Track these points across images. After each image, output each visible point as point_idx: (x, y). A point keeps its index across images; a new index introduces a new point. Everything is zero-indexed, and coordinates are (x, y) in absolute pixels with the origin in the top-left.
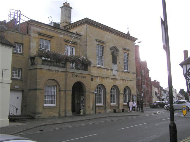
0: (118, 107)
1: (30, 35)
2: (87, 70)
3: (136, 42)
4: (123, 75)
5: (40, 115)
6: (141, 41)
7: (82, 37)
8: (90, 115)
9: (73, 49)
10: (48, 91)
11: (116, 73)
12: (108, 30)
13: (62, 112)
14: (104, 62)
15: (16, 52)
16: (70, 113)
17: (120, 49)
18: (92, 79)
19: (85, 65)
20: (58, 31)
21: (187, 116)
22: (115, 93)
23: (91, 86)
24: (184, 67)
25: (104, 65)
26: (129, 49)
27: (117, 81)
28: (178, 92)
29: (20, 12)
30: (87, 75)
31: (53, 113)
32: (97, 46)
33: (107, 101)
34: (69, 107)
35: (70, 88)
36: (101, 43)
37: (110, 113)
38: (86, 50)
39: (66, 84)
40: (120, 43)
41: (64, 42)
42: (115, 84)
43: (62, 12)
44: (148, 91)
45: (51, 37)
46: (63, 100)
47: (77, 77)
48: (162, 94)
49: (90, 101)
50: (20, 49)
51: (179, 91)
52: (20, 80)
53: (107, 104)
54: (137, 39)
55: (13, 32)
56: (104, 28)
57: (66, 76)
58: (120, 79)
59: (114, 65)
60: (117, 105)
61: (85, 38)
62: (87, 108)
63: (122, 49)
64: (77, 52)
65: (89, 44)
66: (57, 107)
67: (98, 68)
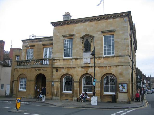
4: (100, 61)
14: (63, 52)
17: (98, 36)
18: (57, 71)
26: (115, 29)
41: (43, 46)
47: (38, 70)
67: (64, 60)
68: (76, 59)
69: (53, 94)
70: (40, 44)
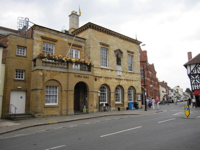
0: (123, 105)
1: (33, 39)
2: (90, 71)
3: (141, 45)
4: (127, 75)
5: (40, 114)
6: (145, 44)
7: (86, 40)
8: (93, 112)
9: (78, 52)
10: (49, 91)
11: (121, 74)
12: (112, 34)
13: (64, 110)
14: (108, 63)
15: (19, 54)
16: (72, 111)
17: (125, 52)
18: (96, 80)
19: (89, 67)
20: (62, 35)
21: (191, 117)
22: (120, 92)
23: (94, 86)
24: (188, 67)
25: (108, 66)
26: (134, 52)
27: (122, 81)
28: (184, 91)
29: (28, 19)
30: (90, 76)
31: (54, 112)
32: (101, 48)
33: (111, 99)
34: (72, 106)
35: (72, 87)
36: (105, 46)
37: (114, 110)
38: (89, 53)
39: (68, 84)
40: (125, 47)
42: (120, 84)
43: (70, 20)
44: (155, 91)
45: (55, 41)
46: (64, 100)
47: (79, 77)
48: (169, 92)
49: (93, 100)
50: (24, 51)
51: (186, 90)
52: (24, 81)
53: (111, 103)
54: (141, 42)
55: (16, 36)
56: (107, 32)
57: (68, 76)
58: (125, 80)
59: (118, 66)
60: (122, 103)
61: (89, 42)
62: (90, 107)
63: (126, 51)
64: (82, 54)
65: (93, 47)
66: (59, 106)
67: (102, 69)
68: (112, 70)
70: (65, 42)
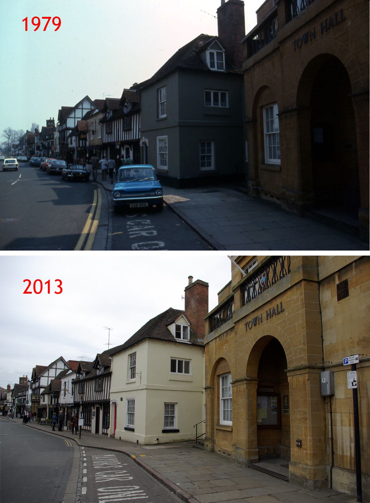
69: (333, 453)
